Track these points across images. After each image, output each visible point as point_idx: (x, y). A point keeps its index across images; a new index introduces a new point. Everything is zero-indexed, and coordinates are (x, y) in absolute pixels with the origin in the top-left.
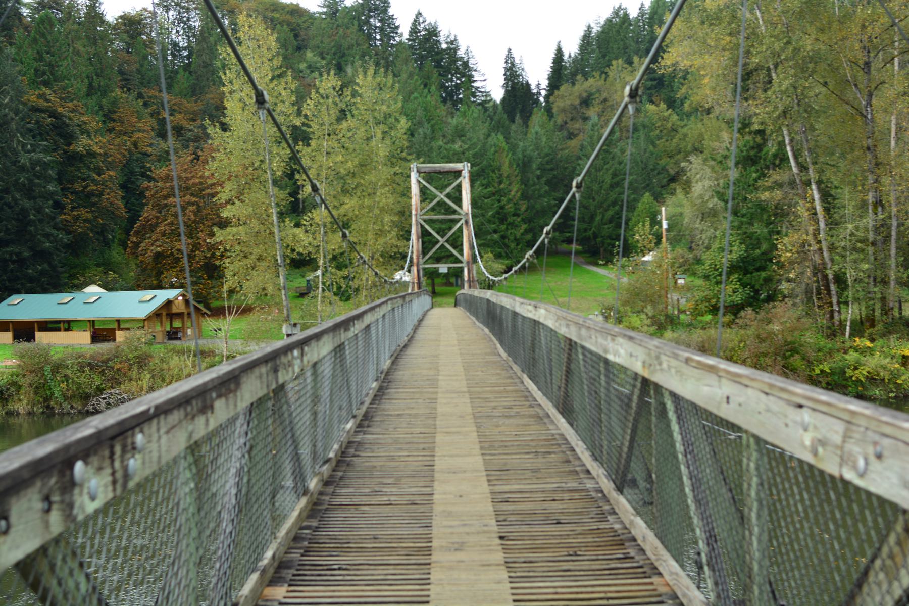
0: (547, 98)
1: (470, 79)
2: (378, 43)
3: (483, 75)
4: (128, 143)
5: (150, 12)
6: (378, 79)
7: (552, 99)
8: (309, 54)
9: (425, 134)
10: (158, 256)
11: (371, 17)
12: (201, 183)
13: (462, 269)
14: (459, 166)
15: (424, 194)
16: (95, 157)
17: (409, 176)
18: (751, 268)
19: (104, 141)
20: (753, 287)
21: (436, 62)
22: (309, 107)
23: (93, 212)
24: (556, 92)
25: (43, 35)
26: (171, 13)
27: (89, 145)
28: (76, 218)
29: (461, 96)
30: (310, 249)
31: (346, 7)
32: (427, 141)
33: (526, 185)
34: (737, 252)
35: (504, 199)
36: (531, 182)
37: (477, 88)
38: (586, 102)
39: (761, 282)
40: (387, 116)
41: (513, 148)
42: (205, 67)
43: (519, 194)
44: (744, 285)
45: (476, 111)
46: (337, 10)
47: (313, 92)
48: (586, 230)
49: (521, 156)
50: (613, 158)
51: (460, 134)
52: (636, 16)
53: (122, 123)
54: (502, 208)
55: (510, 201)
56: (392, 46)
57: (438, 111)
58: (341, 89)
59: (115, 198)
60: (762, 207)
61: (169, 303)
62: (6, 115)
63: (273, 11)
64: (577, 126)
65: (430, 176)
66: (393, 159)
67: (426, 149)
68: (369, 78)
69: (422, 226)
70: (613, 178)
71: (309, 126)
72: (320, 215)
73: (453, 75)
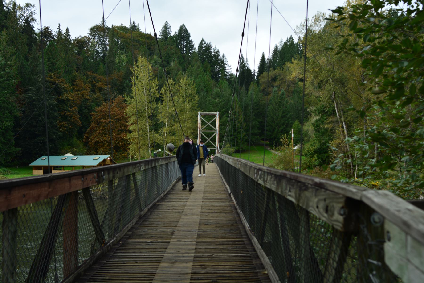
0: (257, 77)
1: (224, 69)
2: (185, 52)
3: (230, 66)
4: (80, 95)
5: (88, 38)
6: (188, 81)
7: (259, 78)
8: (155, 57)
9: (204, 95)
10: (97, 143)
11: (182, 41)
12: (114, 114)
13: (215, 150)
14: (215, 113)
15: (203, 123)
16: (69, 101)
17: (197, 116)
18: (322, 152)
19: (73, 94)
20: (322, 159)
21: (209, 59)
22: (163, 91)
23: (68, 123)
24: (261, 75)
25: (50, 51)
26: (96, 37)
27: (67, 96)
28: (61, 126)
29: (220, 76)
30: (161, 142)
31: (171, 36)
32: (204, 98)
33: (246, 116)
34: (317, 146)
35: (237, 122)
36: (248, 115)
37: (227, 72)
38: (274, 79)
39: (325, 157)
40: (190, 95)
41: (241, 100)
42: (111, 62)
43: (243, 120)
44: (319, 158)
45: (226, 83)
46: (167, 37)
47: (164, 85)
48: (271, 135)
49: (244, 104)
50: (283, 105)
51: (218, 95)
52: (297, 42)
53: (77, 86)
54: (235, 125)
55: (239, 122)
56: (191, 53)
57: (210, 82)
58: (175, 85)
59: (76, 118)
60: (326, 130)
61: (104, 160)
62: (40, 86)
63: (140, 37)
64: (270, 90)
65: (204, 116)
66: (192, 110)
67: (204, 101)
68: (185, 81)
69: (202, 135)
70: (283, 114)
71: (163, 98)
72: (165, 129)
73: (217, 67)
